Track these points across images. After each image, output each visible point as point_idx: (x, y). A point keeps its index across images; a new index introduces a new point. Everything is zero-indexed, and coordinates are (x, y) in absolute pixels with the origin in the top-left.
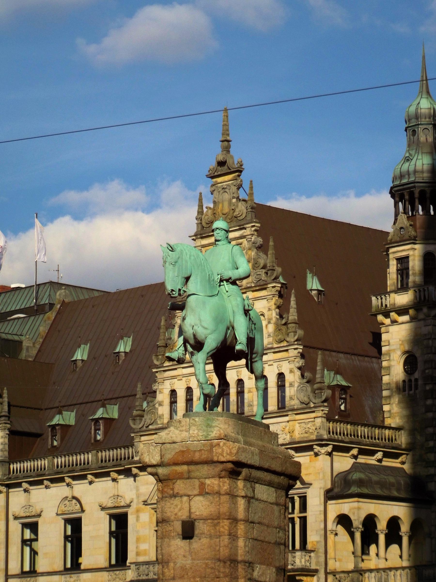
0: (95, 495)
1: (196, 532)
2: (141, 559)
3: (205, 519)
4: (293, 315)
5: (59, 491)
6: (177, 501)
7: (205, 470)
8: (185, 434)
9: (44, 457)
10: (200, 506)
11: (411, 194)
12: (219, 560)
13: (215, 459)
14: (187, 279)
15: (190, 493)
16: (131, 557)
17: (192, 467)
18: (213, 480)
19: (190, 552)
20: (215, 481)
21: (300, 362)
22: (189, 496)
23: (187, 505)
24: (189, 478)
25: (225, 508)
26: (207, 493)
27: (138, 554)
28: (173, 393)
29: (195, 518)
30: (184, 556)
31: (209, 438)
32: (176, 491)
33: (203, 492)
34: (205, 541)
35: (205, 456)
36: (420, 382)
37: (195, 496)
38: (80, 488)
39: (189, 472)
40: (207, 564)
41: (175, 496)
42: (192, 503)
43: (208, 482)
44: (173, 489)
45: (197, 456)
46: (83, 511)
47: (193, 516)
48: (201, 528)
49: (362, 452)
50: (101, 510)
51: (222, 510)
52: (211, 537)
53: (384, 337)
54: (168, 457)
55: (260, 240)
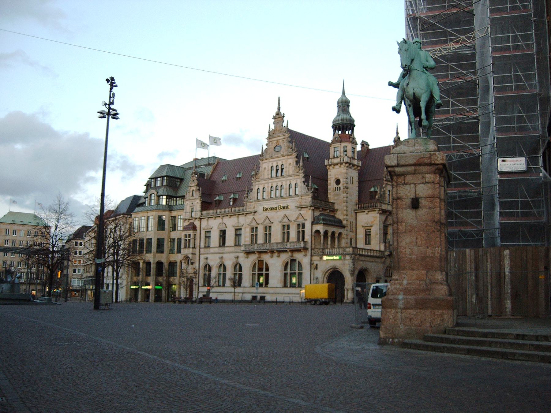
0: (230, 223)
1: (420, 205)
2: (246, 243)
4: (301, 164)
5: (219, 220)
6: (407, 187)
7: (426, 168)
8: (411, 149)
9: (213, 209)
10: (423, 190)
11: (339, 127)
12: (434, 221)
13: (433, 162)
14: (412, 60)
17: (417, 168)
18: (430, 175)
19: (416, 217)
20: (432, 176)
21: (303, 180)
22: (415, 184)
24: (414, 174)
25: (437, 192)
27: (245, 241)
30: (412, 219)
31: (428, 150)
32: (406, 181)
34: (425, 210)
36: (342, 188)
37: (419, 184)
38: (226, 220)
39: (415, 170)
40: (427, 224)
41: (405, 184)
42: (417, 188)
43: (427, 175)
47: (417, 196)
48: (423, 202)
49: (323, 209)
50: (221, 231)
51: (435, 192)
52: (430, 208)
53: (329, 173)
55: (290, 139)
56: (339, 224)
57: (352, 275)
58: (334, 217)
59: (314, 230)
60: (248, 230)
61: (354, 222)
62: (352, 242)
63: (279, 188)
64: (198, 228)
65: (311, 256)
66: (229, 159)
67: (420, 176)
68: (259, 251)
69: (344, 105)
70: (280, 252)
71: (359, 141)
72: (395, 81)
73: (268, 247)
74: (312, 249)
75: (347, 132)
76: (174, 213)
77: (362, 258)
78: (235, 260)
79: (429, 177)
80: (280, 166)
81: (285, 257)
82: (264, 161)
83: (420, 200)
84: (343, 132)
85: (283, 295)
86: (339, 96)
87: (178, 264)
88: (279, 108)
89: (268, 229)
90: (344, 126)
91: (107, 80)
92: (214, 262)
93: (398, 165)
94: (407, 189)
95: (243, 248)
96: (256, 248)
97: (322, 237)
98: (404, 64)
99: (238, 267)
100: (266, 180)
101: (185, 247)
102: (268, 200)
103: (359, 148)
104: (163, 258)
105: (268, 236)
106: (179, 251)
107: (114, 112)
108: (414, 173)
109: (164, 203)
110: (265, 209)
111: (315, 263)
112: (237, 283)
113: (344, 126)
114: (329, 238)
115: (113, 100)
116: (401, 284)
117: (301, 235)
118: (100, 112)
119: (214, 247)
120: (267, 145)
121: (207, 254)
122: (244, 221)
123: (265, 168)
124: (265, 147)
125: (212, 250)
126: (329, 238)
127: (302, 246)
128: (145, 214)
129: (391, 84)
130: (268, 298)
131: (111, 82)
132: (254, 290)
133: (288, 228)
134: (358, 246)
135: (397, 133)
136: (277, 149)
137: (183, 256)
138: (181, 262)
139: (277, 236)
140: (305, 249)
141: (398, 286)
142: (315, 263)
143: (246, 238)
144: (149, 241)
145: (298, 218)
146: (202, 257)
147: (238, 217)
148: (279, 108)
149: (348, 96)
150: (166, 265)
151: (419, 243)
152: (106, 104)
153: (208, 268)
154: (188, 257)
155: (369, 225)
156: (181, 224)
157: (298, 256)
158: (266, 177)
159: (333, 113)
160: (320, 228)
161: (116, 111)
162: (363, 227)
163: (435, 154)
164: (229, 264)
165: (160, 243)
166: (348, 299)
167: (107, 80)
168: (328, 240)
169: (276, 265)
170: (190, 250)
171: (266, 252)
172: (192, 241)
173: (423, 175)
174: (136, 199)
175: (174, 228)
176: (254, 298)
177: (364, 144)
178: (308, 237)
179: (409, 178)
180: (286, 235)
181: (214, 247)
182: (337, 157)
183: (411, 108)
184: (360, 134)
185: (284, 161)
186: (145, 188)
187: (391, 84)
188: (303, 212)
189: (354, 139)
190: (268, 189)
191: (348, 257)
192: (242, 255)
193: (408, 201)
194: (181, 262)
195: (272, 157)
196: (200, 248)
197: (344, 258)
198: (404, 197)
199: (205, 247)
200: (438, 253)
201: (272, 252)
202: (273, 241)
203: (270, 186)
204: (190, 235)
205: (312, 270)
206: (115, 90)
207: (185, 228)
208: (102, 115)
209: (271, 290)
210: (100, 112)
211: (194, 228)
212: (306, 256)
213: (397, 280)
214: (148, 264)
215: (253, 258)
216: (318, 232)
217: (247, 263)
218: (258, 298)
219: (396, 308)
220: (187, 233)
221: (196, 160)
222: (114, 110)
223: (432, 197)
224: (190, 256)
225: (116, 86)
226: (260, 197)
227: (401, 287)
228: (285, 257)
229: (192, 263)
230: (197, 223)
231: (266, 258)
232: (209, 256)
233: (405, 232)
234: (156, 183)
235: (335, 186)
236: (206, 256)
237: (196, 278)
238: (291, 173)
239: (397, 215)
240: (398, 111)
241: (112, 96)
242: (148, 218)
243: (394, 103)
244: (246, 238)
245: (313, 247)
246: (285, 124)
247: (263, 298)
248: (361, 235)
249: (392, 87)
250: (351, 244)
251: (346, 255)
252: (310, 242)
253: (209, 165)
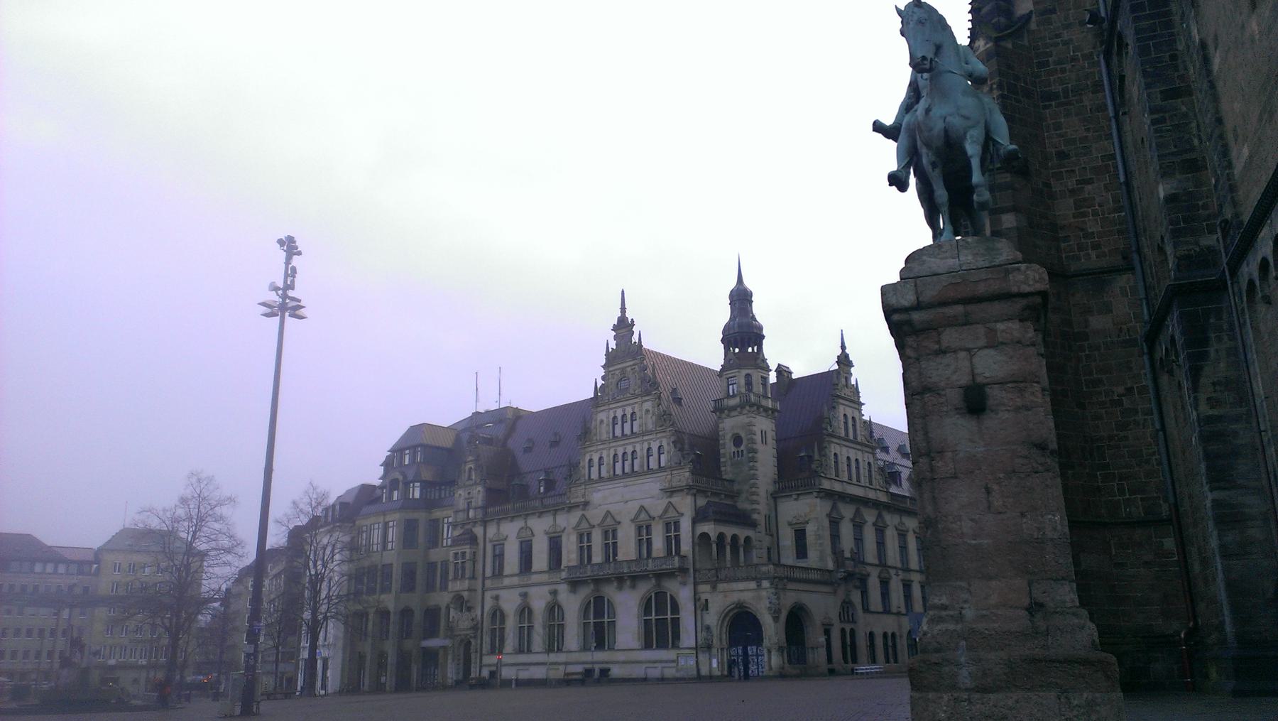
0: (540, 526)
1: (990, 402)
3: (1001, 383)
5: (519, 524)
6: (947, 359)
7: (997, 308)
10: (990, 365)
13: (1015, 289)
15: (971, 346)
16: (564, 563)
17: (970, 308)
20: (1015, 326)
21: (673, 439)
22: (968, 350)
23: (967, 363)
26: (1002, 343)
28: (590, 460)
29: (985, 381)
32: (945, 344)
33: (993, 344)
35: (995, 287)
37: (980, 349)
41: (942, 352)
42: (975, 360)
43: (1000, 326)
44: (938, 342)
45: (982, 289)
46: (533, 534)
47: (979, 379)
48: (995, 394)
54: (929, 294)
56: (744, 519)
57: (776, 619)
58: (734, 507)
59: (698, 532)
60: (574, 538)
61: (773, 515)
62: (773, 553)
63: (630, 457)
64: (481, 541)
65: (695, 584)
66: (535, 410)
67: (980, 329)
68: (596, 582)
69: (741, 299)
70: (635, 579)
71: (773, 367)
72: (889, 121)
73: (610, 570)
74: (695, 570)
75: (750, 350)
76: (437, 514)
77: (791, 586)
78: (549, 598)
79: (1011, 329)
81: (644, 588)
83: (987, 390)
84: (744, 350)
85: (644, 666)
86: (733, 283)
87: (443, 610)
88: (623, 309)
89: (610, 534)
90: (743, 334)
91: (281, 242)
92: (510, 602)
93: (918, 307)
94: (948, 365)
95: (564, 575)
96: (589, 574)
97: (714, 546)
98: (919, 55)
99: (554, 609)
100: (603, 442)
101: (455, 578)
102: (610, 479)
103: (773, 378)
104: (414, 601)
105: (611, 548)
106: (444, 587)
107: (294, 304)
108: (966, 322)
109: (417, 495)
111: (703, 597)
112: (555, 642)
113: (743, 334)
114: (728, 549)
115: (293, 282)
116: (960, 618)
117: (673, 542)
118: (263, 304)
119: (512, 576)
120: (603, 378)
121: (498, 589)
122: (567, 521)
123: (602, 421)
124: (600, 382)
125: (507, 582)
126: (728, 549)
127: (677, 565)
128: (381, 519)
129: (878, 127)
130: (616, 671)
131: (290, 247)
132: (587, 657)
133: (648, 533)
134: (783, 561)
135: (843, 347)
136: (623, 385)
137: (451, 595)
138: (448, 608)
139: (627, 549)
140: (683, 570)
141: (951, 627)
142: (703, 597)
143: (570, 554)
144: (387, 570)
145: (666, 511)
146: (488, 595)
148: (623, 309)
149: (749, 283)
150: (418, 617)
151: (997, 503)
152: (276, 289)
153: (498, 615)
154: (462, 597)
155: (801, 520)
156: (448, 534)
157: (672, 586)
158: (604, 437)
159: (722, 314)
160: (709, 528)
161: (299, 301)
162: (790, 524)
163: (1018, 269)
164: (539, 603)
165: (409, 574)
166: (771, 668)
167: (281, 242)
168: (721, 557)
169: (627, 609)
170: (466, 584)
171: (607, 580)
172: (468, 566)
173: (992, 325)
174: (366, 490)
175: (434, 540)
176: (588, 673)
177: (782, 371)
178: (686, 547)
179: (950, 337)
180: (644, 542)
181: (512, 576)
182: (734, 396)
183: (937, 171)
184: (775, 352)
186: (381, 471)
187: (878, 127)
188: (675, 500)
189: (764, 360)
190: (608, 459)
191: (766, 584)
192: (563, 589)
193: (954, 396)
194: (448, 608)
195: (615, 401)
196: (484, 578)
197: (759, 586)
198: (942, 384)
199: (494, 574)
200: (1055, 529)
201: (620, 580)
202: (620, 557)
203: (612, 453)
204: (464, 553)
205: (699, 612)
206: (296, 261)
207: (456, 542)
208: (268, 310)
209: (620, 657)
210: (263, 304)
211: (473, 540)
212: (684, 584)
213: (944, 607)
214: (384, 614)
215: (585, 592)
216: (705, 536)
217: (572, 604)
218: (597, 672)
219: (954, 687)
220: (459, 550)
221: (476, 414)
222: (293, 299)
223: (1018, 382)
224: (465, 594)
225: (299, 253)
226: (594, 476)
227: (959, 627)
228: (644, 588)
229: (469, 609)
230: (478, 531)
231: (610, 591)
232: (502, 593)
233: (955, 477)
234: (402, 459)
235: (733, 449)
236: (495, 593)
237: (475, 637)
238: (650, 426)
239: (926, 433)
240: (902, 187)
241: (291, 273)
242: (386, 525)
243: (893, 166)
244: (570, 554)
245: (698, 566)
246: (635, 338)
247: (605, 672)
248: (787, 539)
249: (880, 135)
250: (769, 559)
251: (761, 579)
252: (691, 557)
253: (501, 421)
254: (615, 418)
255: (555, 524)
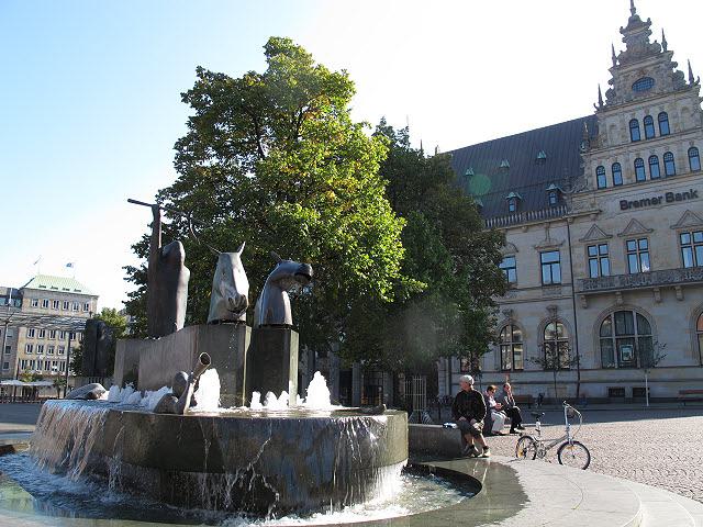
80: (655, 118)
82: (607, 114)
110: (625, 205)
147: (547, 228)
185: (666, 105)
209: (665, 375)
231: (642, 304)
254: (633, 122)
255: (548, 238)
